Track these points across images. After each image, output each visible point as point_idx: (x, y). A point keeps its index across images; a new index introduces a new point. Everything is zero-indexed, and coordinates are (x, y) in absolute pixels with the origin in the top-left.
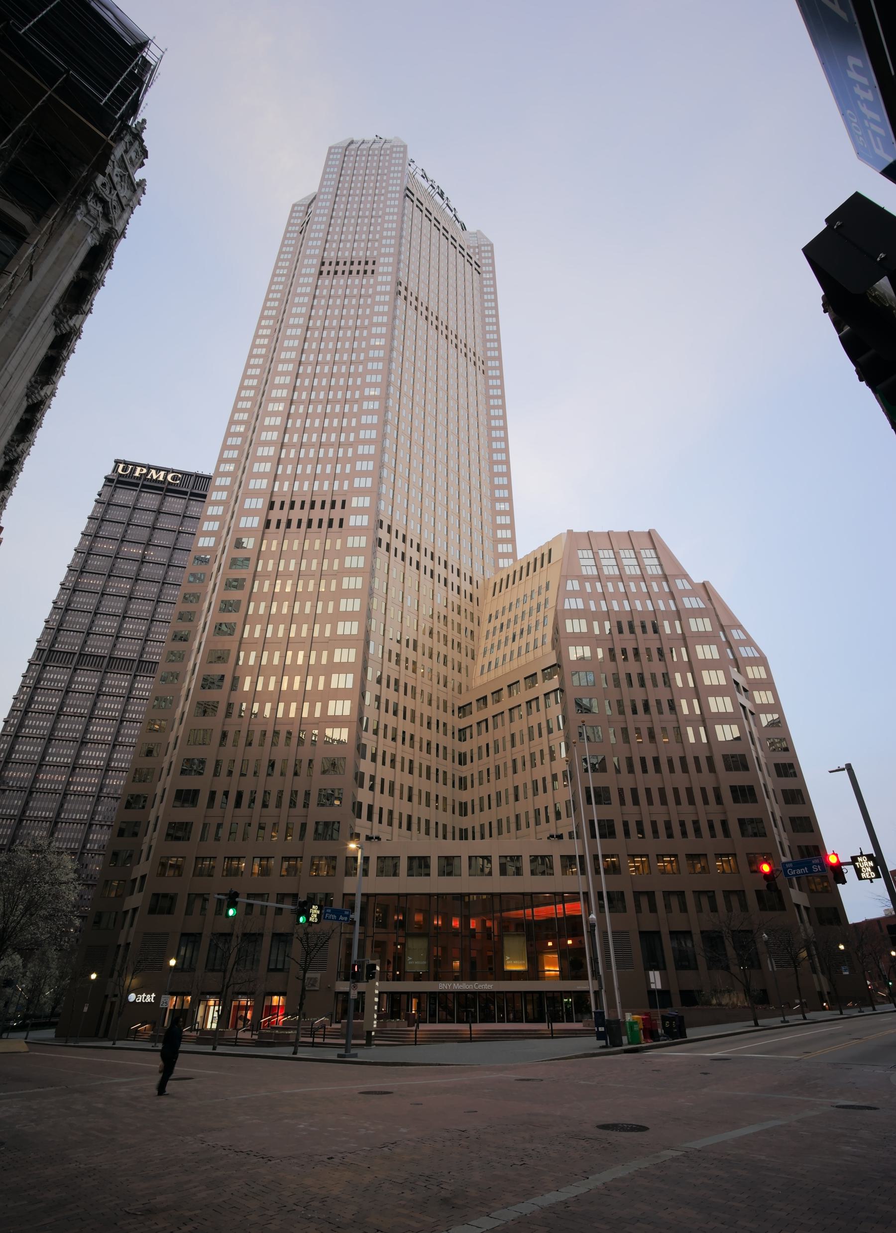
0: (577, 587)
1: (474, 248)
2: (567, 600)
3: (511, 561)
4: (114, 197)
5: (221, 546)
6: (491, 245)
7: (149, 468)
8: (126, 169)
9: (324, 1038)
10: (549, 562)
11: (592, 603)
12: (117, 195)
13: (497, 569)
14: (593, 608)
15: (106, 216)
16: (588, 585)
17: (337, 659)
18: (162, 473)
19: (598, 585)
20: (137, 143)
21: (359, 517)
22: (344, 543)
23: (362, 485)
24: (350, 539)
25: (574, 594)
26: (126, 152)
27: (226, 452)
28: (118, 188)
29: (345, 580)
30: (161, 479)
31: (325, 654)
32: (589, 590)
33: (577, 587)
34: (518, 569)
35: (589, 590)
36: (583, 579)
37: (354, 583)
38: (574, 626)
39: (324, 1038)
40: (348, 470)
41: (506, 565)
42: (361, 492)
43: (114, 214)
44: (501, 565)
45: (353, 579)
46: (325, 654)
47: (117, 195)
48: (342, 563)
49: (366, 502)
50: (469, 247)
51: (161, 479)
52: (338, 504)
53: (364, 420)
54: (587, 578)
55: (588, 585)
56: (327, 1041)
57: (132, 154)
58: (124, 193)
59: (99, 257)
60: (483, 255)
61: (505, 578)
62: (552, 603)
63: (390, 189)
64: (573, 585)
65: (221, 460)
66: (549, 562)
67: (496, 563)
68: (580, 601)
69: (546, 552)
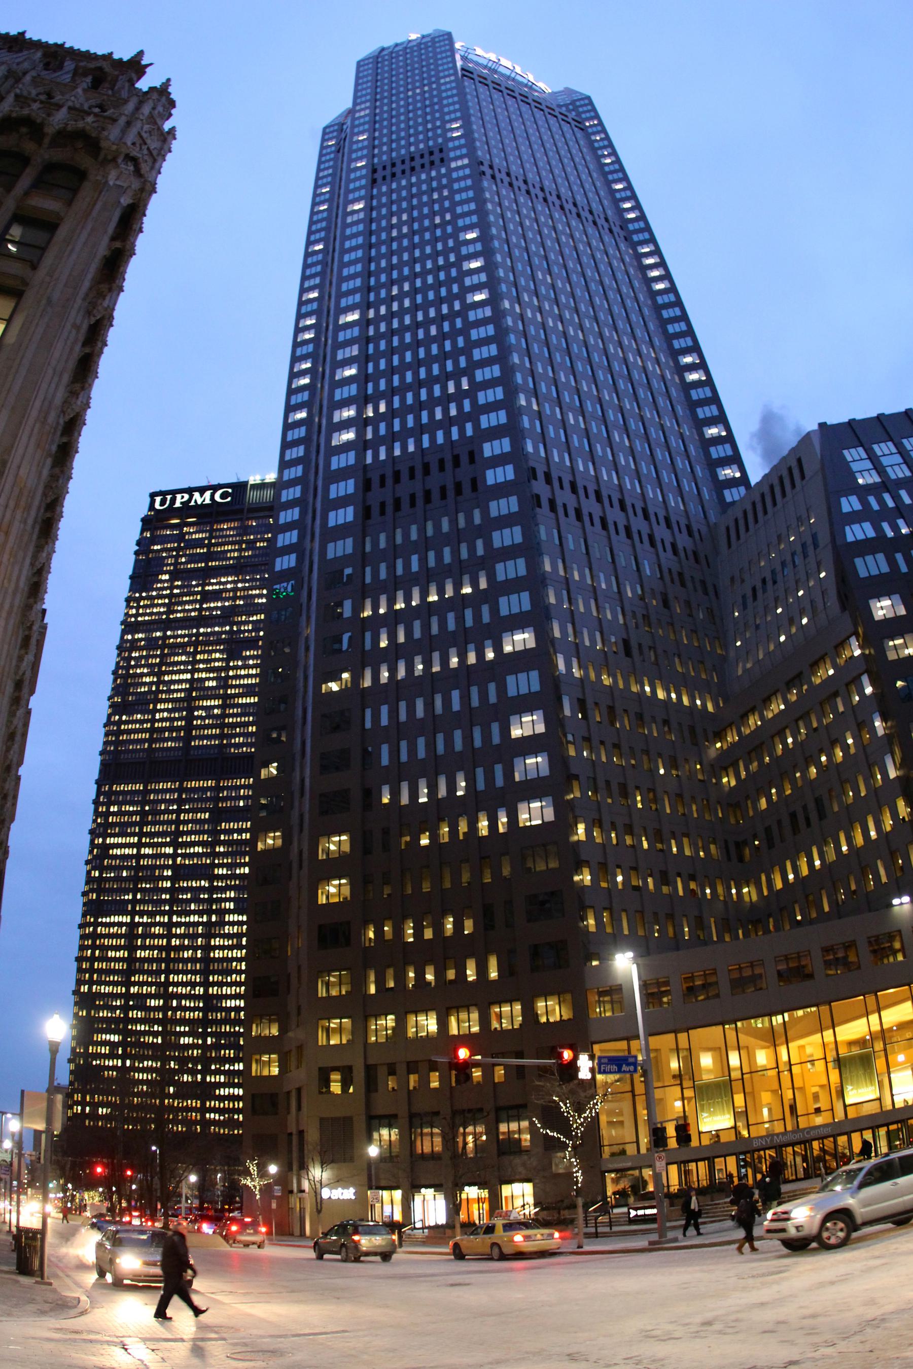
0: (857, 506)
1: (566, 105)
2: (847, 528)
3: (742, 489)
4: (145, 152)
5: (307, 562)
6: (589, 98)
7: (190, 491)
8: (155, 123)
9: (611, 1227)
10: (803, 477)
11: (885, 526)
12: (148, 149)
13: (725, 506)
14: (890, 534)
15: (138, 172)
16: (872, 500)
17: (512, 692)
18: (208, 494)
19: (887, 497)
20: (164, 99)
21: (506, 532)
22: (485, 512)
23: (503, 502)
24: (511, 680)
25: (855, 517)
26: (154, 108)
27: (286, 472)
28: (148, 141)
29: (493, 505)
30: (208, 501)
31: (492, 687)
32: (875, 506)
33: (857, 506)
34: (758, 499)
35: (875, 506)
36: (863, 492)
37: (511, 536)
38: (871, 566)
39: (611, 1227)
40: (477, 520)
41: (737, 498)
42: (495, 433)
43: (144, 168)
44: (729, 499)
45: (514, 598)
46: (492, 687)
47: (148, 149)
48: (488, 544)
49: (505, 445)
50: (560, 106)
51: (208, 501)
52: (464, 459)
53: (482, 398)
54: (868, 489)
55: (872, 500)
56: (615, 1229)
57: (160, 109)
58: (154, 144)
59: (129, 221)
60: (581, 110)
61: (740, 515)
62: (824, 538)
63: (457, 198)
64: (849, 504)
65: (284, 465)
66: (803, 477)
67: (721, 498)
68: (867, 526)
69: (794, 464)
